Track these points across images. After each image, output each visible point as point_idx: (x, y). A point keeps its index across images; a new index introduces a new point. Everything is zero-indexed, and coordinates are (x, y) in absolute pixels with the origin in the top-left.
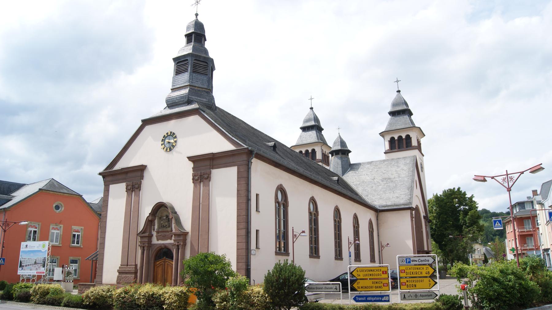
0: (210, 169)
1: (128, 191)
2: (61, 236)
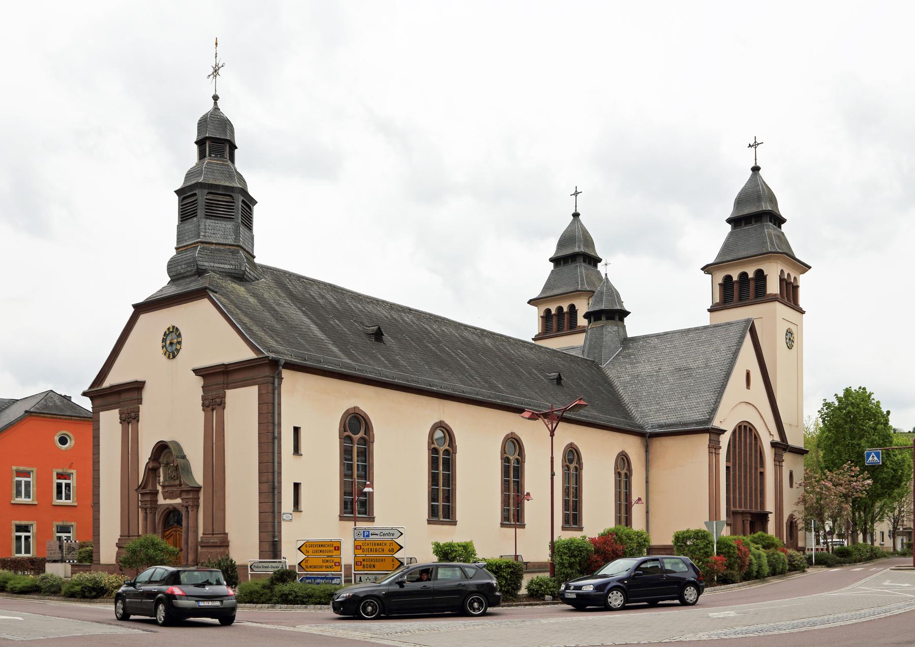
0: (224, 389)
1: (123, 422)
2: (75, 489)
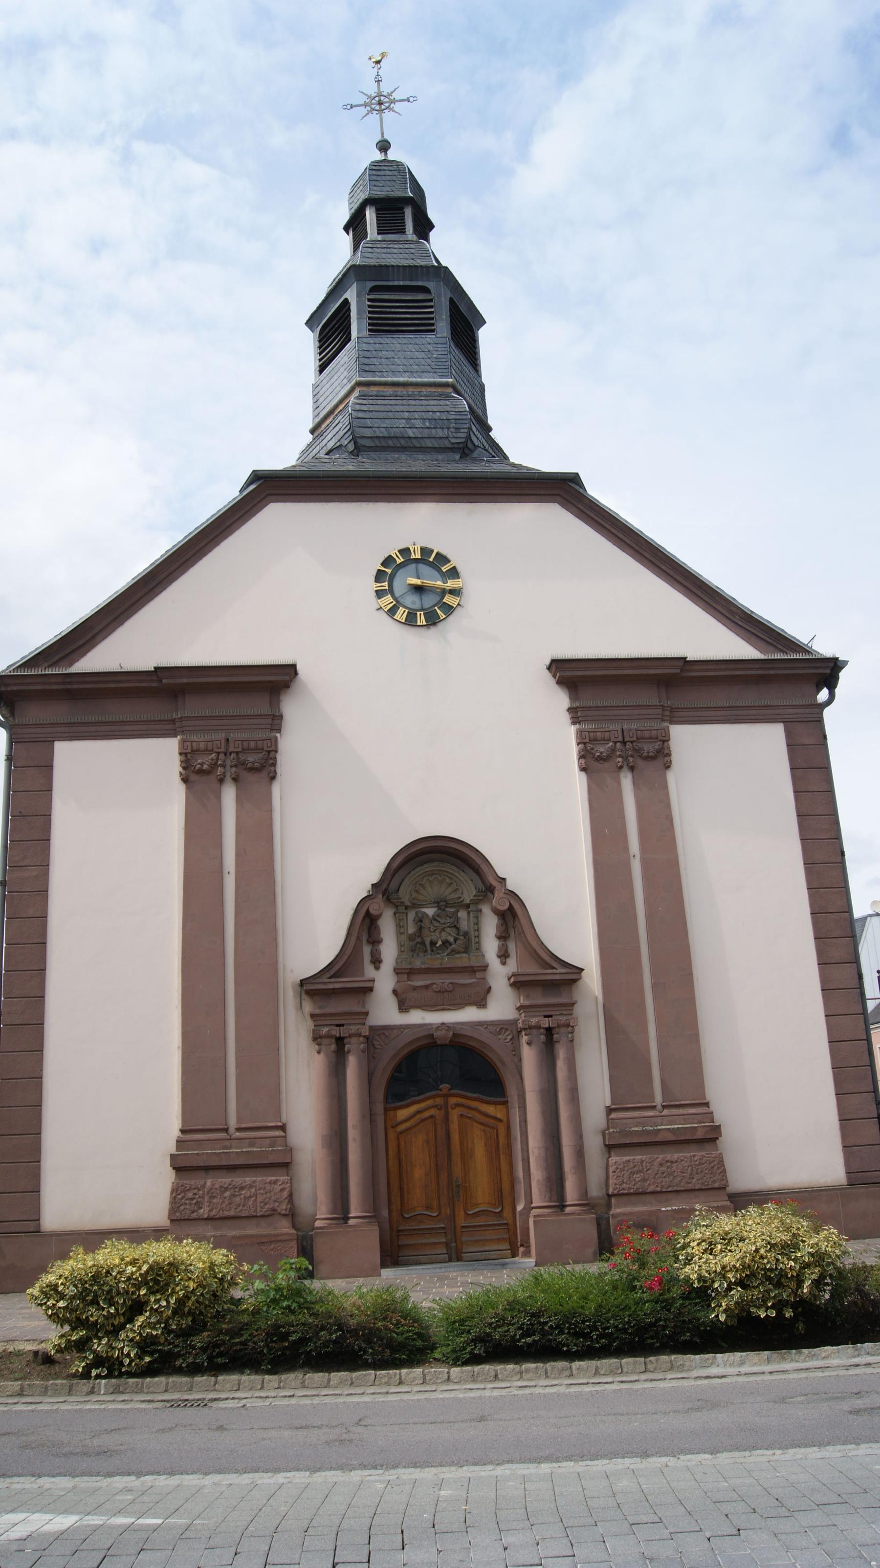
1: (193, 777)
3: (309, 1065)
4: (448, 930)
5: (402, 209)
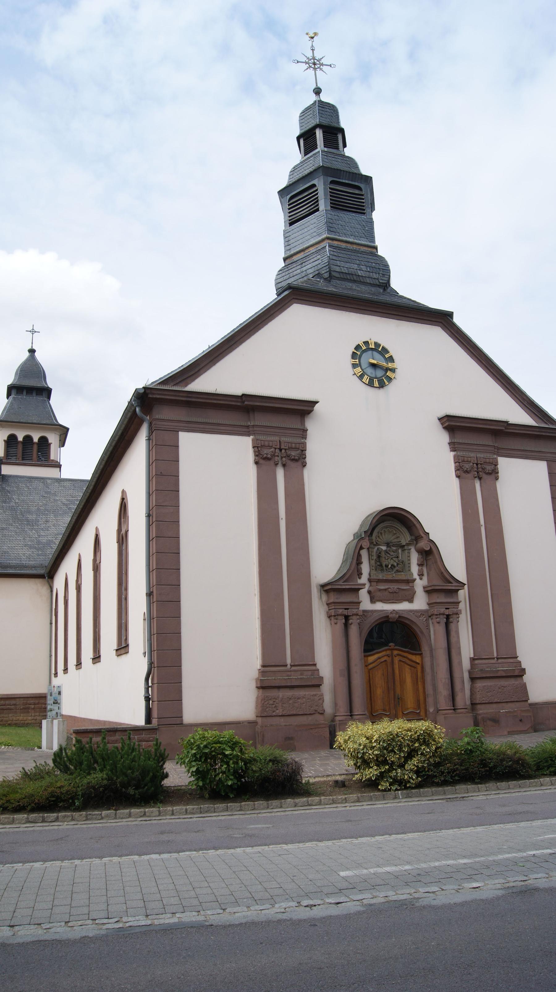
1: (261, 461)
3: (326, 631)
4: (394, 559)
5: (336, 134)
